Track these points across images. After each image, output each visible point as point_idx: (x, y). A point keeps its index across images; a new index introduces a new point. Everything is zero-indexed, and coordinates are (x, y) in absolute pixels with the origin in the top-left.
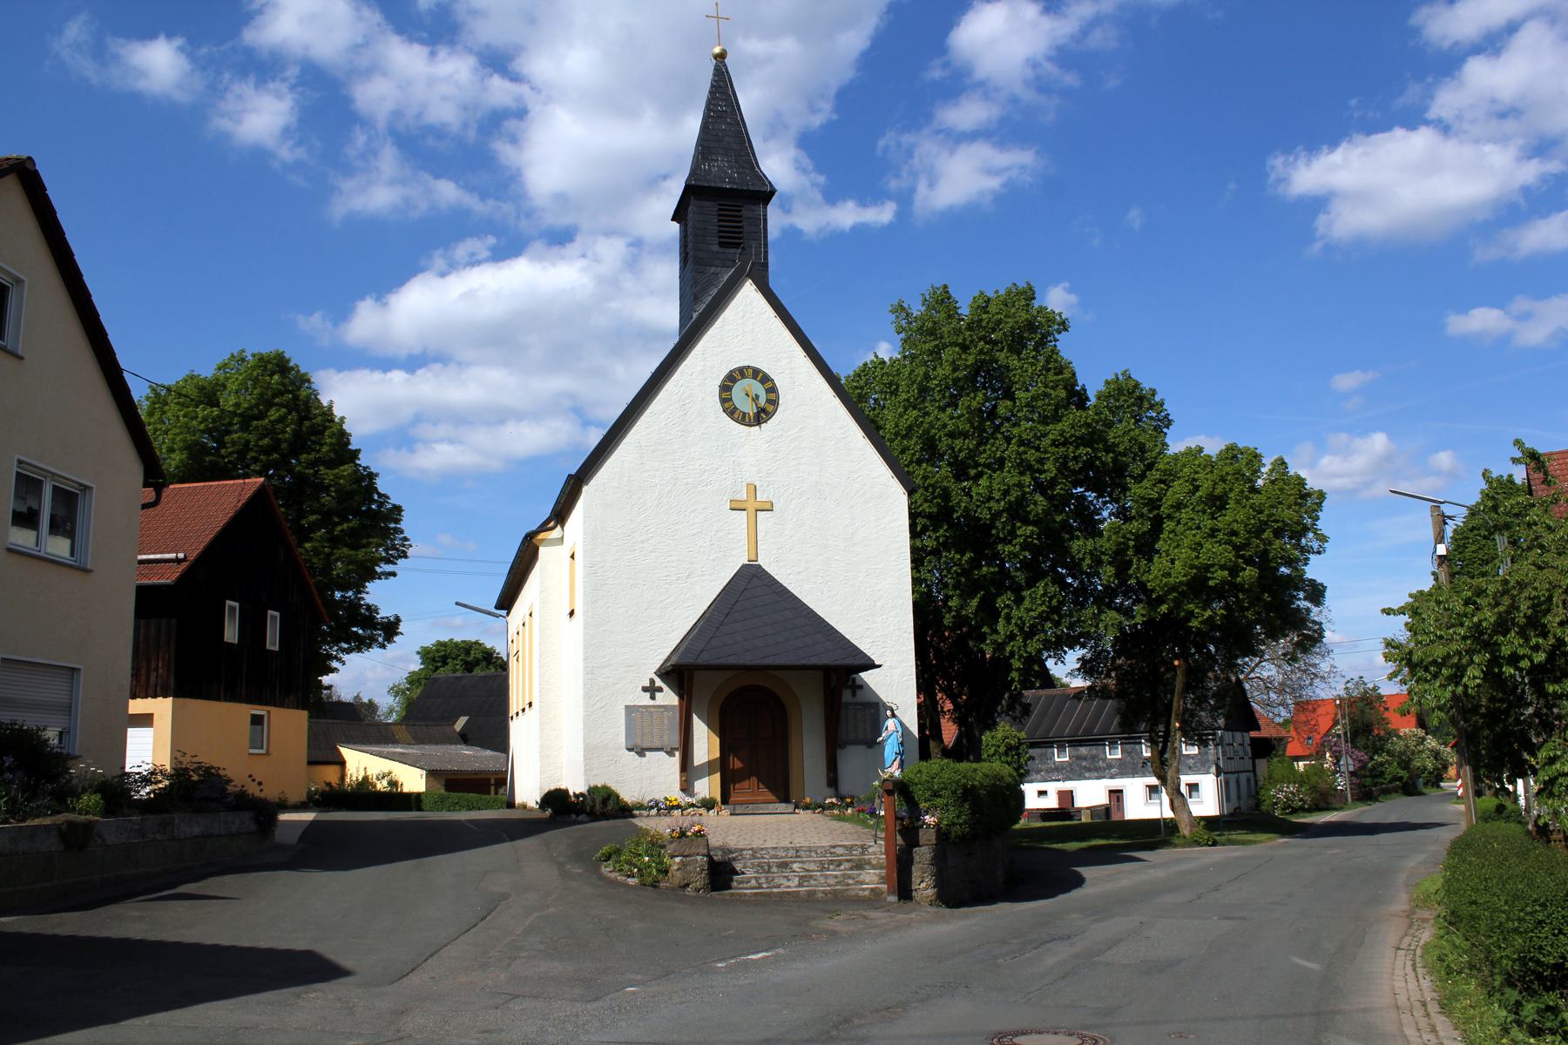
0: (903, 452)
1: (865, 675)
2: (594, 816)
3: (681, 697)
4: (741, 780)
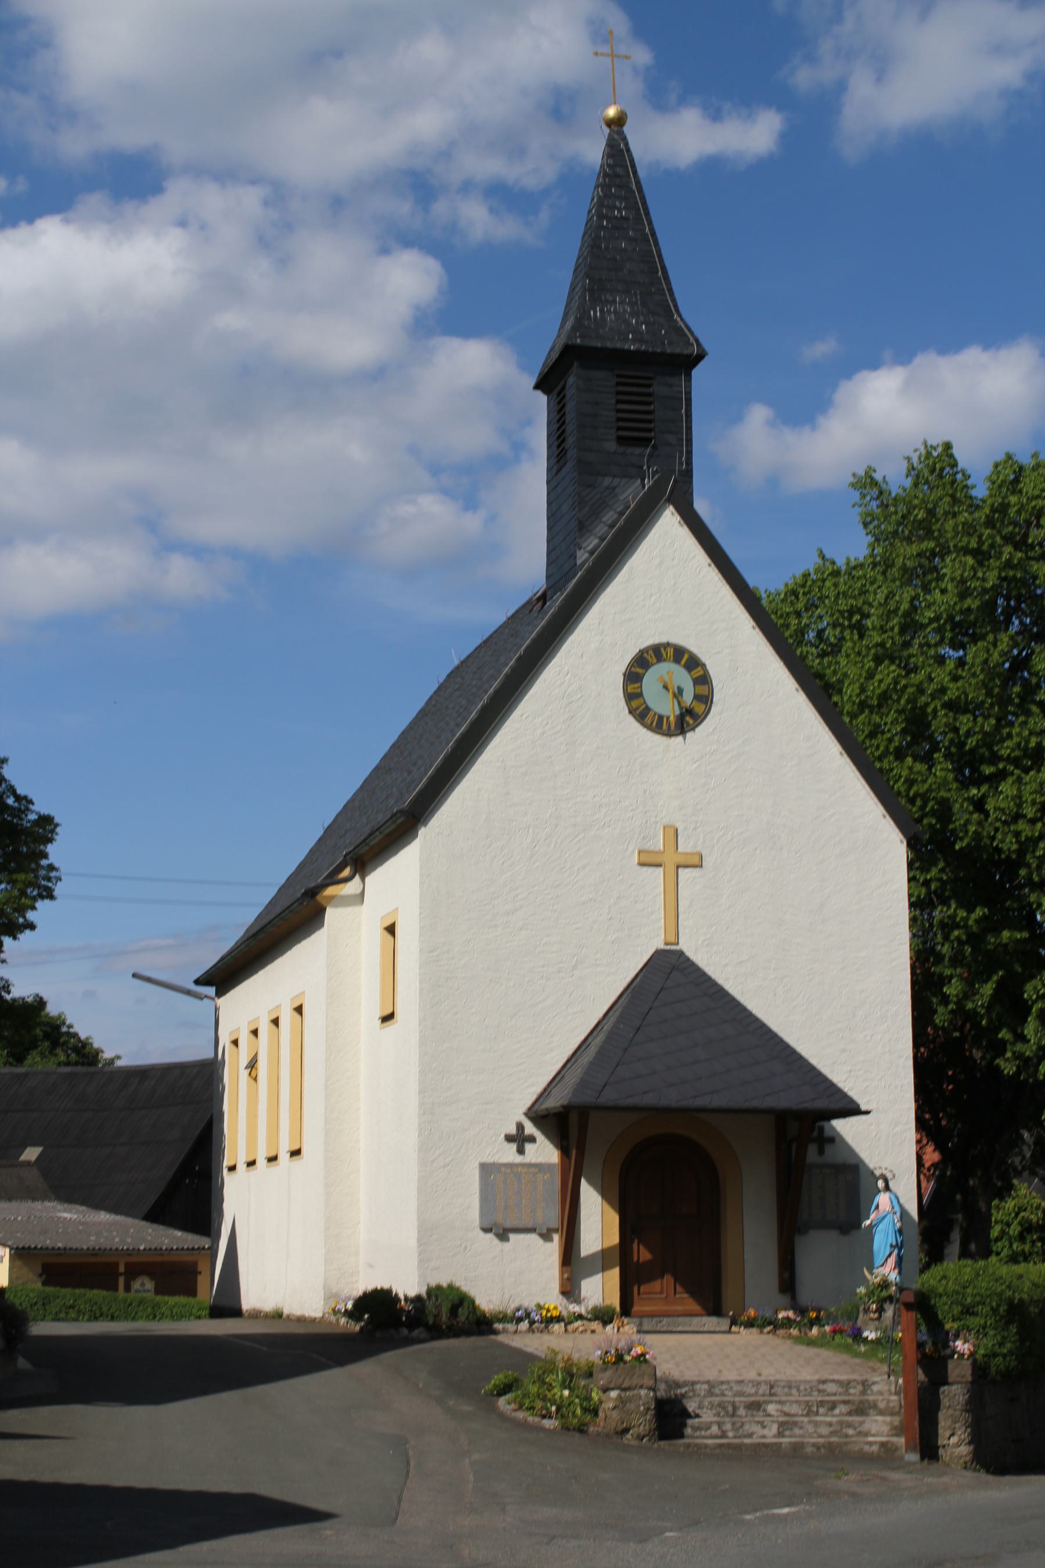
0: (872, 735)
1: (840, 1125)
2: (437, 1332)
3: (564, 1151)
4: (650, 1279)
